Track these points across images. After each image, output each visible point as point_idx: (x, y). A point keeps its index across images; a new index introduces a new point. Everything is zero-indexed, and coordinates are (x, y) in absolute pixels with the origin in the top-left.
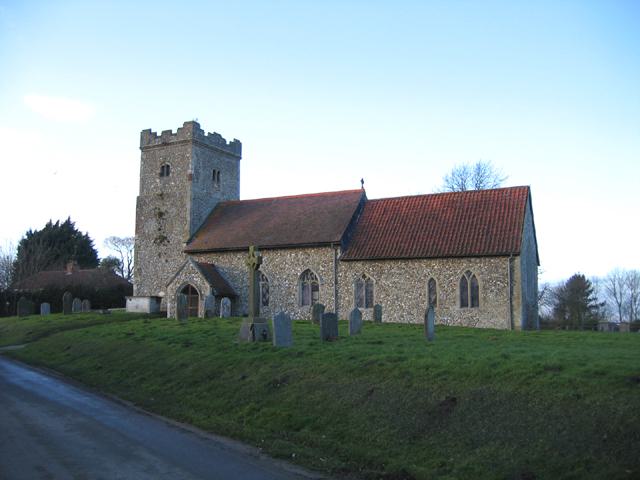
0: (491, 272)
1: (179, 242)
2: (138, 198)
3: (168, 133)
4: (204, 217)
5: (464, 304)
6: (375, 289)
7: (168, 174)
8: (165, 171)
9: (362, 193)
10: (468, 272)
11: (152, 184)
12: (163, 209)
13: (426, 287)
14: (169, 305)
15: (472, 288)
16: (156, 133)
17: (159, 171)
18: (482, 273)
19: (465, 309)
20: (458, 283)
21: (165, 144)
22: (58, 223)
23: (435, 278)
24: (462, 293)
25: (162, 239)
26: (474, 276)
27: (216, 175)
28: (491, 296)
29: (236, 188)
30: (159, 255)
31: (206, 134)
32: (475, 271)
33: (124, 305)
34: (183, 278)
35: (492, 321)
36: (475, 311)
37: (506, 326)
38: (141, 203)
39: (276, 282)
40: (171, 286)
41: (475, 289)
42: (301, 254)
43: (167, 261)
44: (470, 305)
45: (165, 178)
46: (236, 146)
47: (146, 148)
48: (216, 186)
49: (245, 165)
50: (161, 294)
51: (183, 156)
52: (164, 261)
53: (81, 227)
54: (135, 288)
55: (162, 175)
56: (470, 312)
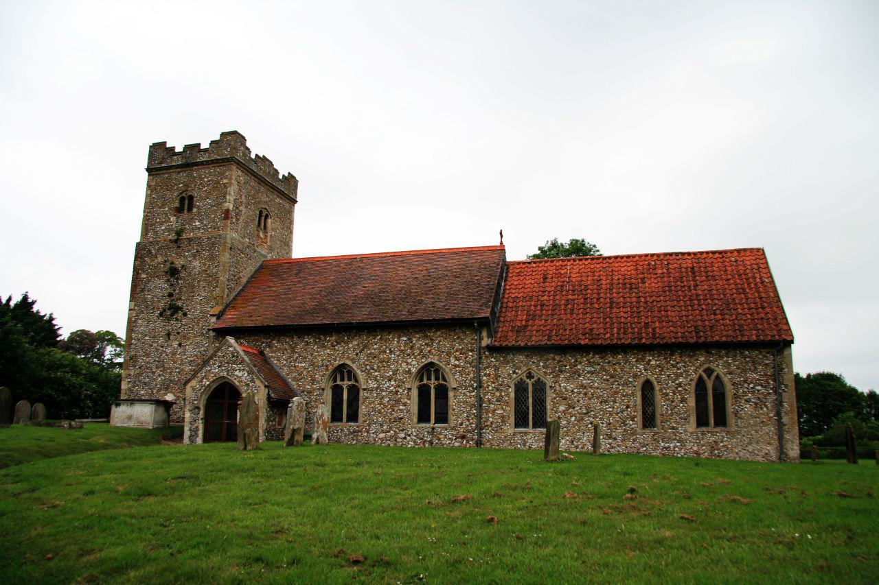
0: (745, 371)
1: (204, 314)
2: (138, 244)
3: (193, 148)
4: (244, 280)
5: (702, 421)
6: (550, 396)
7: (190, 209)
8: (186, 204)
9: (501, 250)
10: (709, 372)
11: (162, 223)
12: (179, 262)
13: (639, 394)
14: (187, 415)
15: (715, 396)
16: (173, 149)
17: (177, 204)
18: (730, 373)
19: (704, 429)
20: (692, 388)
21: (187, 166)
22: (9, 299)
23: (653, 379)
24: (517, 399)
25: (174, 310)
26: (718, 377)
27: (263, 217)
28: (748, 408)
29: (287, 243)
30: (168, 335)
31: (253, 156)
32: (720, 370)
33: (107, 414)
34: (215, 370)
35: (750, 448)
36: (720, 433)
37: (122, 398)
38: (141, 252)
39: (373, 384)
40: (193, 383)
41: (720, 398)
42: (418, 341)
43: (180, 345)
44: (712, 422)
45: (186, 215)
46: (291, 180)
47: (157, 169)
48: (262, 235)
49: (300, 212)
50: (169, 397)
51: (218, 182)
52: (175, 344)
53: (42, 308)
54: (124, 386)
55: (179, 210)
56: (713, 435)
